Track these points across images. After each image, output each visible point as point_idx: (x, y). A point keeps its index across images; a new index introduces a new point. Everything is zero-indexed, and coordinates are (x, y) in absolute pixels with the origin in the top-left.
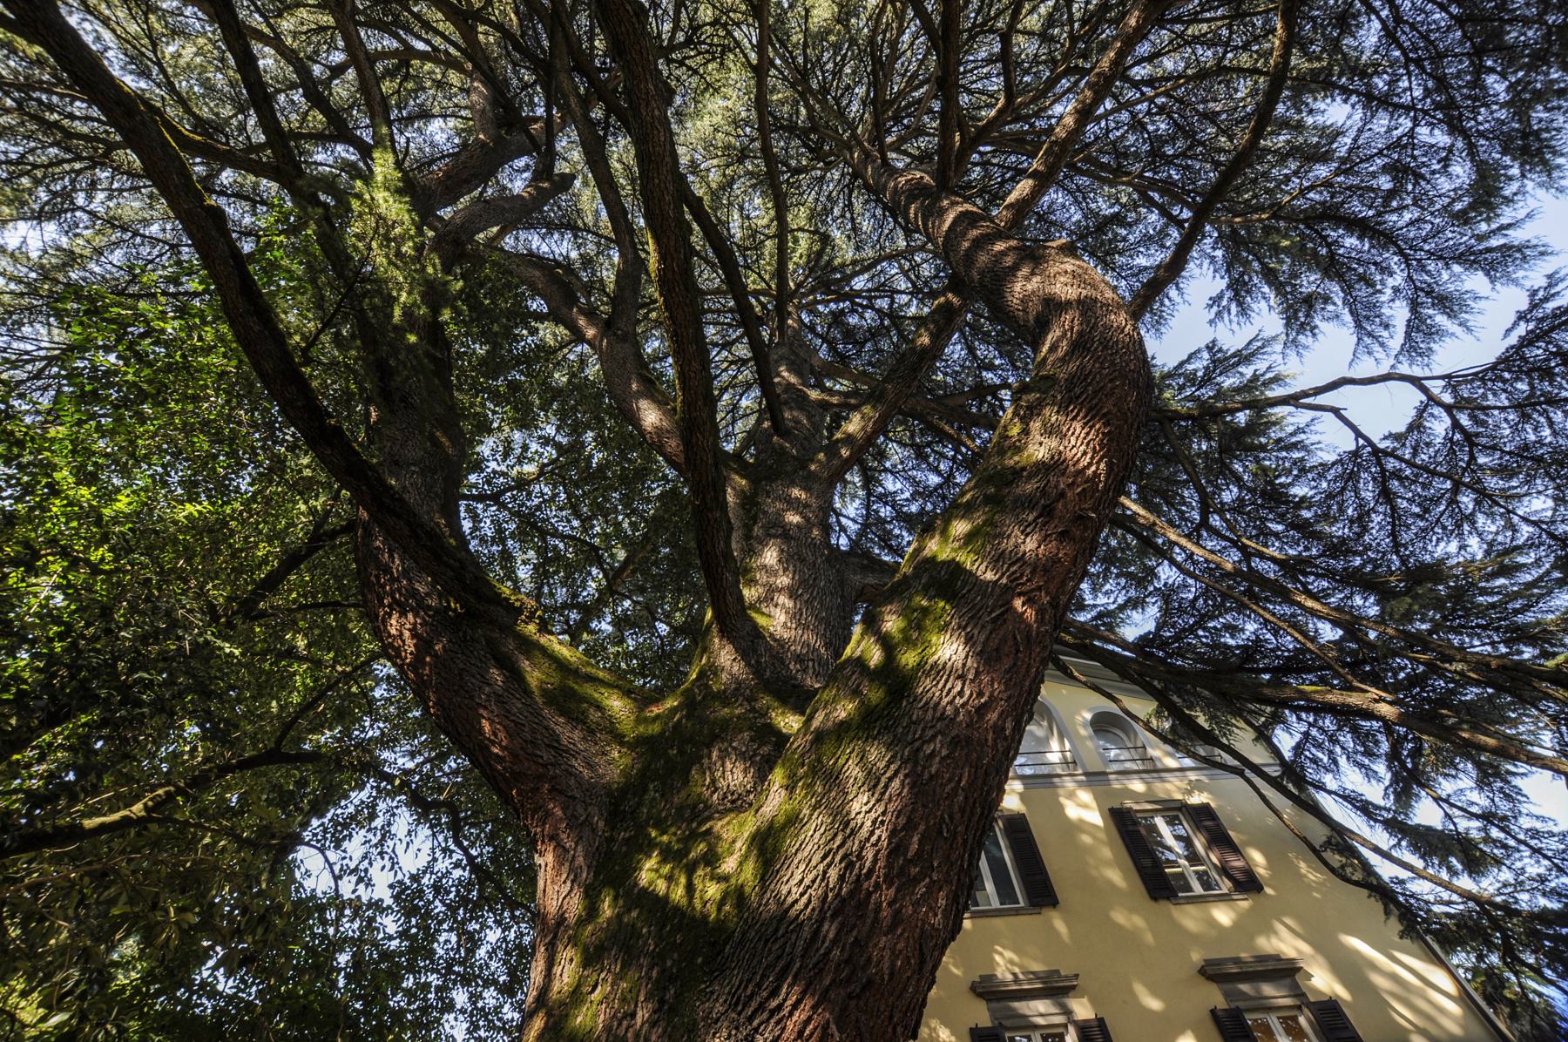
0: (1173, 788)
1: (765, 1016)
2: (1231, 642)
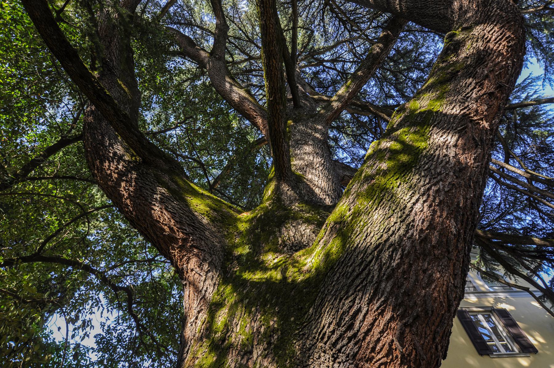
0: (490, 301)
1: (345, 342)
2: (519, 227)
